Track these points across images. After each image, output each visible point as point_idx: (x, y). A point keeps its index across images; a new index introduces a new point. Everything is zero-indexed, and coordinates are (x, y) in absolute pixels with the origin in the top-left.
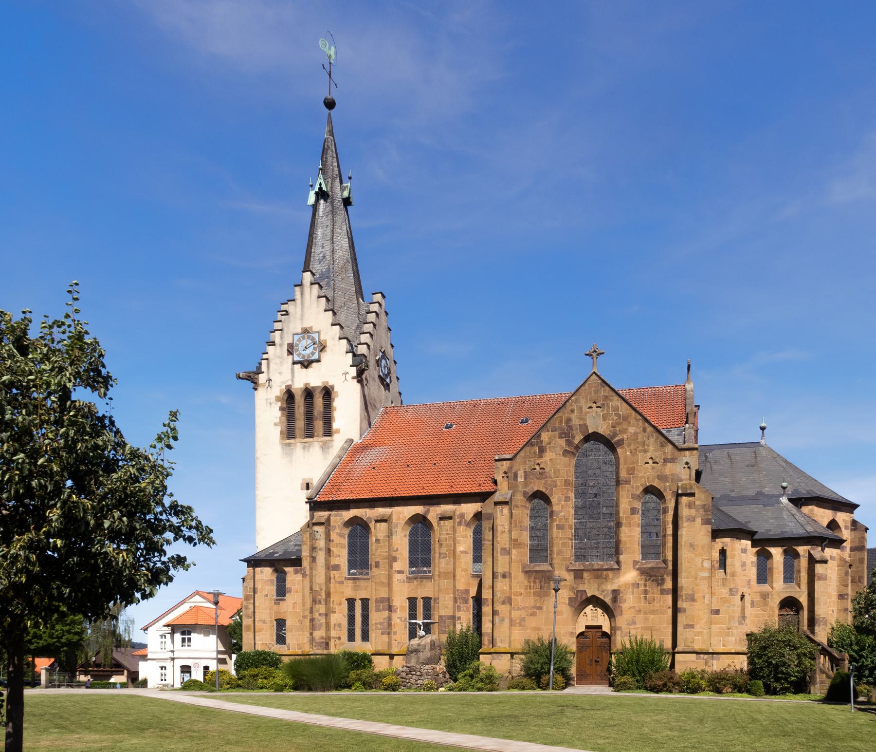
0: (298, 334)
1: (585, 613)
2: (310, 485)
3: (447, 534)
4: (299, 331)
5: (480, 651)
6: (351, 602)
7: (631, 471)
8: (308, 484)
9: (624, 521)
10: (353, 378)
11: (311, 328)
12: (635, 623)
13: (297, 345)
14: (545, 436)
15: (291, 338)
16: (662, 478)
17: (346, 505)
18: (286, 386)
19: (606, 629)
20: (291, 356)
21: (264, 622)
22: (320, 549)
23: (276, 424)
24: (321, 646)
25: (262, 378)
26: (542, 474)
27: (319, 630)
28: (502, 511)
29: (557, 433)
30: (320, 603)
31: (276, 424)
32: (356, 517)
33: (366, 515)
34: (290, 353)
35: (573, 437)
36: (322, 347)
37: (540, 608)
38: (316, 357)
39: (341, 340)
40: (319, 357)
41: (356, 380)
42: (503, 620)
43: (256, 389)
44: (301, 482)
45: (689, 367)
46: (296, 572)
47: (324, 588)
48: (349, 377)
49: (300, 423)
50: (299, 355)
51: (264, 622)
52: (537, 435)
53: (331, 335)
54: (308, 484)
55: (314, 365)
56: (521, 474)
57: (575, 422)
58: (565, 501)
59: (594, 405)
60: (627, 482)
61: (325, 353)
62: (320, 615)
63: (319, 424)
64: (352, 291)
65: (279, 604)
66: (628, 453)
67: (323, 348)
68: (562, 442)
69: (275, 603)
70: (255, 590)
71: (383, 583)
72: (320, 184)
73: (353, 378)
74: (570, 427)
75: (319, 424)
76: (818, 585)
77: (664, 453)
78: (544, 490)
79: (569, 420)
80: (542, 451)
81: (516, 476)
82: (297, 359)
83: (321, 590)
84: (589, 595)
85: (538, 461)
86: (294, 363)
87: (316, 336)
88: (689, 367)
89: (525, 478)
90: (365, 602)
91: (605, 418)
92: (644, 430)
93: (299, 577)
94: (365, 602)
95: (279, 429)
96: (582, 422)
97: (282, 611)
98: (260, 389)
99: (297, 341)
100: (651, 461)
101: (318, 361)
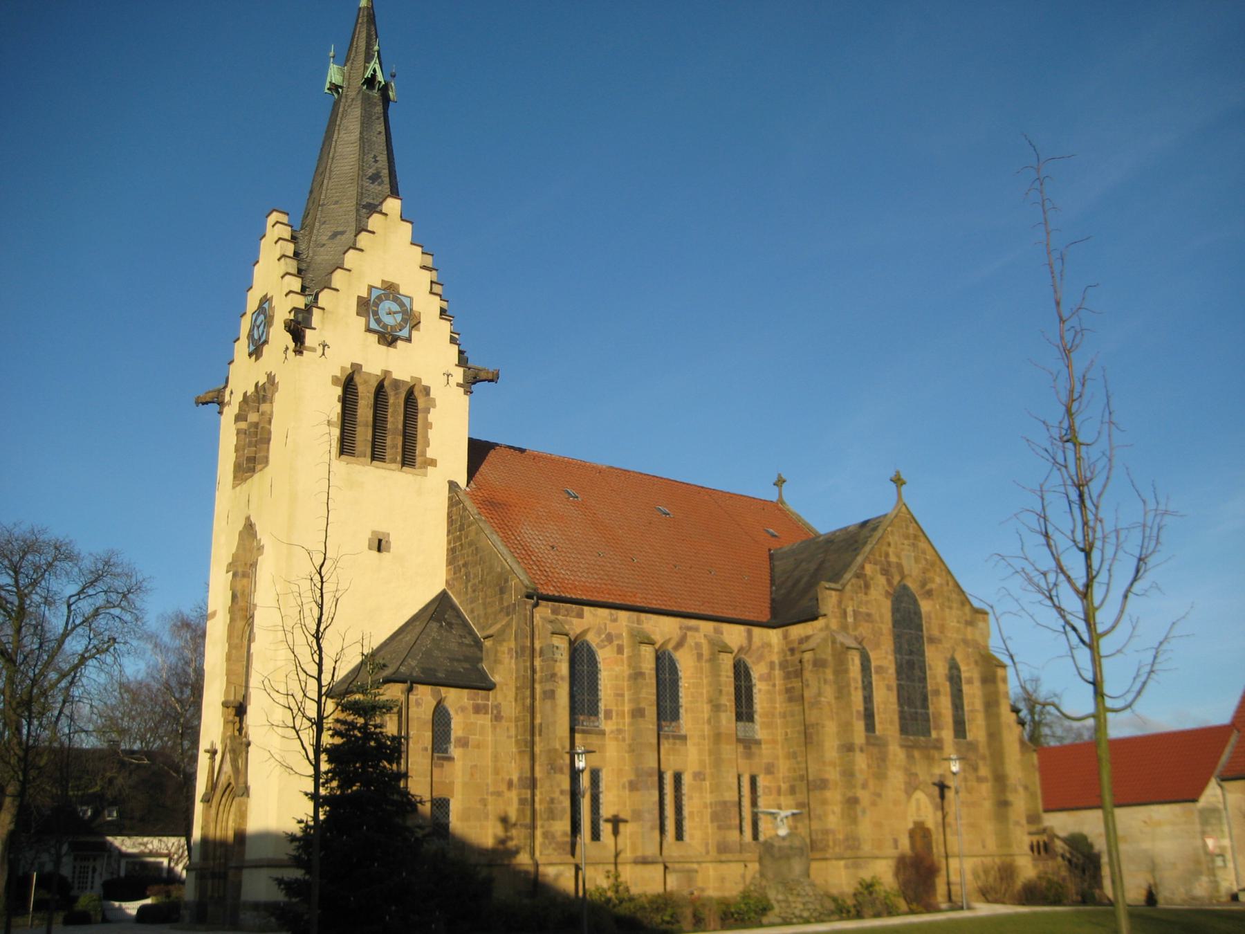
2: (383, 542)
3: (728, 677)
7: (942, 628)
8: (380, 541)
10: (459, 385)
18: (353, 365)
22: (562, 678)
24: (564, 850)
27: (561, 819)
29: (878, 568)
30: (561, 771)
33: (606, 629)
35: (893, 578)
42: (864, 811)
44: (369, 535)
48: (453, 381)
49: (364, 434)
50: (378, 321)
53: (427, 306)
54: (380, 541)
57: (893, 559)
60: (940, 641)
62: (562, 792)
63: (394, 441)
68: (882, 580)
71: (651, 743)
74: (889, 563)
75: (394, 441)
79: (887, 555)
82: (373, 325)
89: (855, 619)
91: (917, 560)
92: (948, 584)
96: (898, 561)
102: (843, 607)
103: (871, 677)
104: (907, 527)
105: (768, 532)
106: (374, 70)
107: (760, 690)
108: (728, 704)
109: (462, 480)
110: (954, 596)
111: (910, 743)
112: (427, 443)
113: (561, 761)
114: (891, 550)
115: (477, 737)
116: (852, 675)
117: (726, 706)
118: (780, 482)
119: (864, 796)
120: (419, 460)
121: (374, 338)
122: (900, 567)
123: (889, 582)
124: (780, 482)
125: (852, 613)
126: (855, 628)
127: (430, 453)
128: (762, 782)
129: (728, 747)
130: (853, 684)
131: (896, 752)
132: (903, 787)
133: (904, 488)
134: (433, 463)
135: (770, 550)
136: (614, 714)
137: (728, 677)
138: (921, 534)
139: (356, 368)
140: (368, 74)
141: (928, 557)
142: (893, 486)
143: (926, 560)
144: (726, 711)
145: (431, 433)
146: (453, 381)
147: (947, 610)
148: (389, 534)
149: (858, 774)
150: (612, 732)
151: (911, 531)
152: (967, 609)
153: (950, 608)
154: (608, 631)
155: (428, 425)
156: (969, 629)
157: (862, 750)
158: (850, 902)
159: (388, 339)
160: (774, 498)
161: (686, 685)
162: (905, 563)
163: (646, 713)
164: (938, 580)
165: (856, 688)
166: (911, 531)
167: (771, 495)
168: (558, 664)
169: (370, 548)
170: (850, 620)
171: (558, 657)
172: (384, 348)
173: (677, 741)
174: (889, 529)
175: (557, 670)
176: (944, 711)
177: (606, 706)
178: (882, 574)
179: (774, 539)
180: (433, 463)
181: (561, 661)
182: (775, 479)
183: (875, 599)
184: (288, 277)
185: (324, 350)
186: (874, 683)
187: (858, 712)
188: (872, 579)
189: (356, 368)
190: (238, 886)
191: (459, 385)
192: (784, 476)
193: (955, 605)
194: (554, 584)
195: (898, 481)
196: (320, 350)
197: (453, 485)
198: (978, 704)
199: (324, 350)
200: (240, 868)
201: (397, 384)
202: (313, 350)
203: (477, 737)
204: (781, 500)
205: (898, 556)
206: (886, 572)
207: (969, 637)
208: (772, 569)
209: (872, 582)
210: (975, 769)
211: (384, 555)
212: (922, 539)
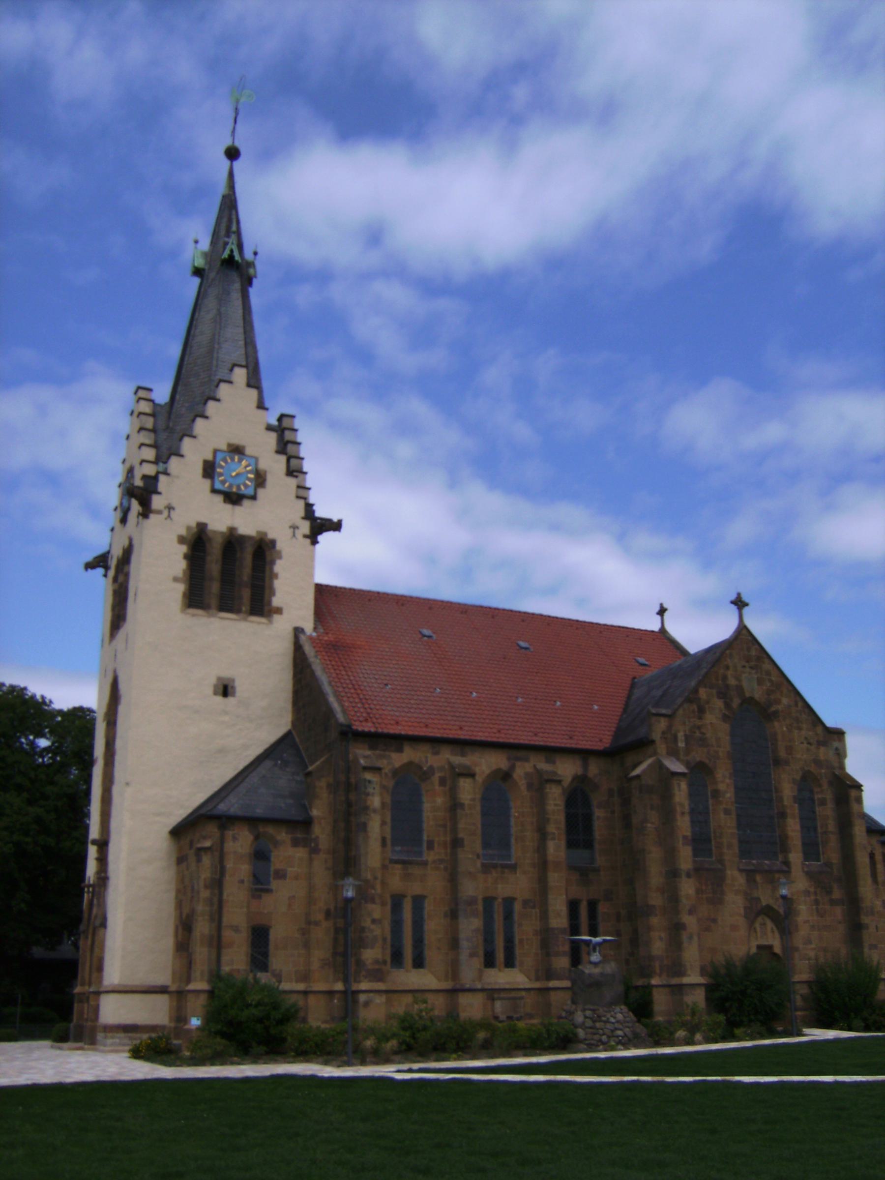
0: (257, 463)
3: (556, 805)
6: (397, 902)
7: (790, 749)
9: (788, 811)
10: (305, 536)
12: (810, 942)
14: (703, 693)
16: (817, 762)
17: (398, 741)
19: (777, 950)
21: (236, 929)
22: (375, 811)
23: (176, 579)
25: (157, 502)
26: (703, 742)
27: (372, 948)
28: (679, 785)
29: (714, 691)
31: (176, 579)
32: (410, 764)
33: (427, 762)
37: (714, 921)
38: (250, 492)
42: (691, 938)
44: (213, 681)
46: (296, 843)
47: (379, 875)
48: (299, 533)
51: (236, 929)
52: (696, 691)
56: (681, 735)
57: (732, 682)
59: (747, 664)
60: (787, 763)
65: (260, 897)
66: (785, 729)
69: (253, 897)
70: (222, 871)
72: (232, 251)
74: (727, 687)
77: (817, 734)
78: (707, 761)
79: (725, 678)
80: (701, 711)
81: (675, 738)
83: (376, 878)
84: (764, 904)
85: (698, 722)
89: (687, 744)
90: (509, 902)
91: (760, 682)
92: (796, 705)
93: (300, 853)
94: (592, 906)
95: (181, 588)
97: (266, 912)
100: (805, 742)
101: (254, 498)
102: (673, 732)
103: (707, 801)
104: (749, 649)
105: (637, 662)
106: (232, 251)
107: (598, 817)
108: (556, 832)
109: (308, 626)
110: (804, 716)
111: (752, 868)
112: (273, 593)
113: (373, 891)
114: (730, 673)
115: (296, 869)
116: (677, 799)
117: (554, 834)
118: (662, 611)
119: (690, 921)
120: (266, 608)
121: (219, 498)
122: (740, 689)
123: (727, 705)
124: (662, 611)
125: (683, 738)
126: (688, 751)
127: (276, 602)
128: (603, 908)
129: (556, 875)
130: (678, 809)
131: (735, 877)
132: (742, 911)
133: (746, 610)
134: (279, 611)
135: (634, 678)
136: (436, 845)
137: (556, 805)
138: (765, 656)
139: (202, 528)
140: (226, 255)
141: (773, 679)
142: (734, 608)
143: (770, 681)
144: (553, 839)
145: (277, 584)
146: (299, 533)
147: (796, 732)
148: (233, 680)
149: (684, 901)
150: (434, 862)
151: (753, 653)
152: (819, 729)
153: (800, 729)
154: (429, 764)
155: (276, 576)
156: (822, 749)
157: (688, 875)
158: (169, 1042)
159: (233, 498)
160: (656, 627)
161: (516, 814)
162: (745, 684)
163: (466, 843)
164: (785, 701)
165: (683, 813)
166: (753, 653)
167: (653, 625)
168: (370, 798)
169: (215, 693)
170: (681, 744)
171: (370, 790)
172: (229, 507)
173: (506, 871)
174: (728, 652)
175: (369, 803)
176: (790, 833)
177: (428, 836)
178: (719, 698)
179: (641, 668)
180: (279, 611)
181: (373, 794)
182: (657, 609)
183: (711, 723)
184: (143, 448)
185: (169, 512)
186: (711, 808)
187: (685, 837)
188: (708, 702)
189: (202, 528)
190: (97, 1009)
191: (305, 536)
192: (665, 606)
193: (804, 726)
194: (375, 720)
195: (739, 603)
196: (166, 513)
197: (298, 631)
198: (832, 826)
199: (169, 512)
200: (98, 994)
201: (243, 539)
202: (159, 512)
203: (296, 869)
204: (663, 630)
205: (738, 679)
206: (723, 694)
207: (822, 757)
208: (629, 697)
209: (707, 706)
210: (829, 892)
211: (230, 700)
212: (766, 661)
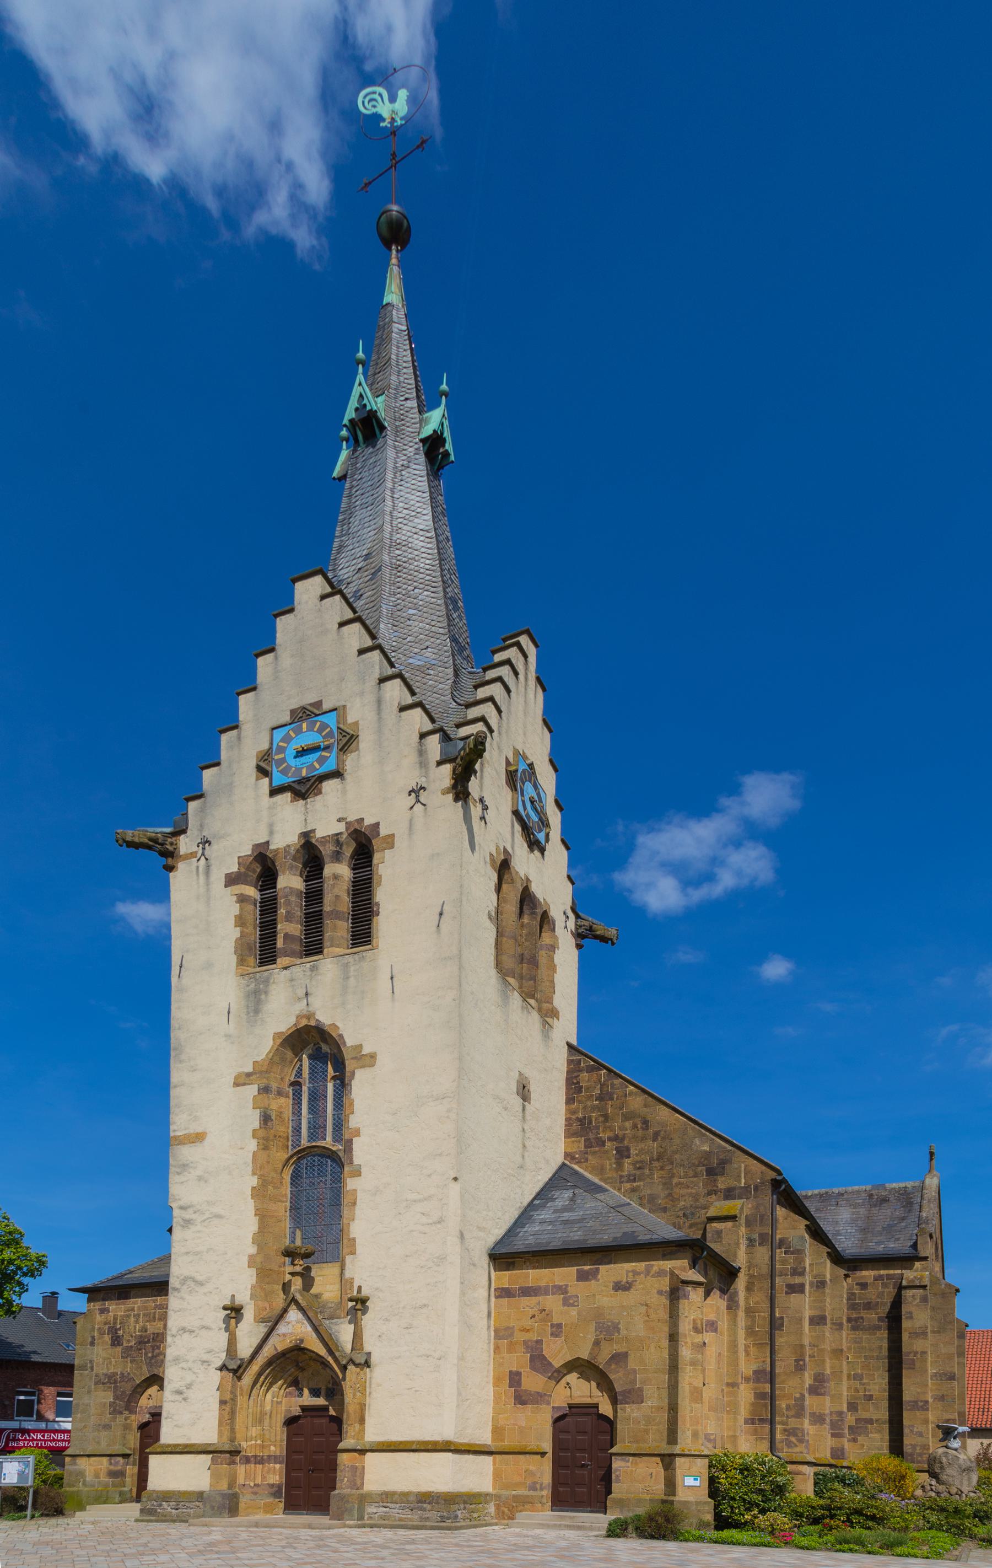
1: (568, 1384)
4: (287, 718)
5: (613, 1450)
10: (445, 792)
11: (319, 704)
13: (281, 750)
15: (267, 738)
20: (266, 780)
34: (263, 772)
36: (345, 740)
38: (330, 765)
39: (404, 714)
40: (340, 762)
41: (450, 797)
43: (170, 868)
45: (932, 1154)
50: (285, 772)
55: (329, 786)
58: (507, 1353)
61: (354, 755)
64: (426, 517)
67: (348, 741)
73: (445, 792)
76: (908, 1418)
82: (279, 779)
86: (274, 792)
87: (331, 720)
88: (932, 1154)
98: (181, 866)
99: (282, 740)
101: (337, 774)
